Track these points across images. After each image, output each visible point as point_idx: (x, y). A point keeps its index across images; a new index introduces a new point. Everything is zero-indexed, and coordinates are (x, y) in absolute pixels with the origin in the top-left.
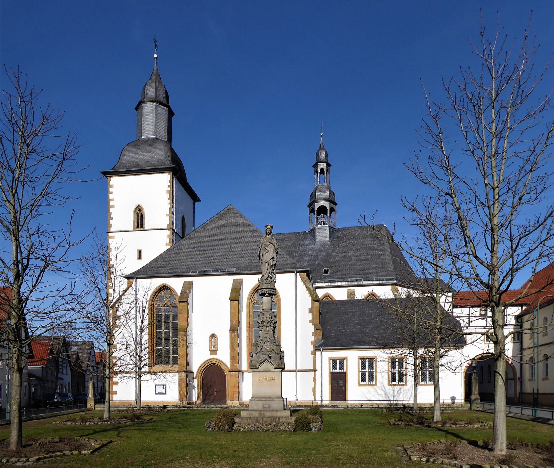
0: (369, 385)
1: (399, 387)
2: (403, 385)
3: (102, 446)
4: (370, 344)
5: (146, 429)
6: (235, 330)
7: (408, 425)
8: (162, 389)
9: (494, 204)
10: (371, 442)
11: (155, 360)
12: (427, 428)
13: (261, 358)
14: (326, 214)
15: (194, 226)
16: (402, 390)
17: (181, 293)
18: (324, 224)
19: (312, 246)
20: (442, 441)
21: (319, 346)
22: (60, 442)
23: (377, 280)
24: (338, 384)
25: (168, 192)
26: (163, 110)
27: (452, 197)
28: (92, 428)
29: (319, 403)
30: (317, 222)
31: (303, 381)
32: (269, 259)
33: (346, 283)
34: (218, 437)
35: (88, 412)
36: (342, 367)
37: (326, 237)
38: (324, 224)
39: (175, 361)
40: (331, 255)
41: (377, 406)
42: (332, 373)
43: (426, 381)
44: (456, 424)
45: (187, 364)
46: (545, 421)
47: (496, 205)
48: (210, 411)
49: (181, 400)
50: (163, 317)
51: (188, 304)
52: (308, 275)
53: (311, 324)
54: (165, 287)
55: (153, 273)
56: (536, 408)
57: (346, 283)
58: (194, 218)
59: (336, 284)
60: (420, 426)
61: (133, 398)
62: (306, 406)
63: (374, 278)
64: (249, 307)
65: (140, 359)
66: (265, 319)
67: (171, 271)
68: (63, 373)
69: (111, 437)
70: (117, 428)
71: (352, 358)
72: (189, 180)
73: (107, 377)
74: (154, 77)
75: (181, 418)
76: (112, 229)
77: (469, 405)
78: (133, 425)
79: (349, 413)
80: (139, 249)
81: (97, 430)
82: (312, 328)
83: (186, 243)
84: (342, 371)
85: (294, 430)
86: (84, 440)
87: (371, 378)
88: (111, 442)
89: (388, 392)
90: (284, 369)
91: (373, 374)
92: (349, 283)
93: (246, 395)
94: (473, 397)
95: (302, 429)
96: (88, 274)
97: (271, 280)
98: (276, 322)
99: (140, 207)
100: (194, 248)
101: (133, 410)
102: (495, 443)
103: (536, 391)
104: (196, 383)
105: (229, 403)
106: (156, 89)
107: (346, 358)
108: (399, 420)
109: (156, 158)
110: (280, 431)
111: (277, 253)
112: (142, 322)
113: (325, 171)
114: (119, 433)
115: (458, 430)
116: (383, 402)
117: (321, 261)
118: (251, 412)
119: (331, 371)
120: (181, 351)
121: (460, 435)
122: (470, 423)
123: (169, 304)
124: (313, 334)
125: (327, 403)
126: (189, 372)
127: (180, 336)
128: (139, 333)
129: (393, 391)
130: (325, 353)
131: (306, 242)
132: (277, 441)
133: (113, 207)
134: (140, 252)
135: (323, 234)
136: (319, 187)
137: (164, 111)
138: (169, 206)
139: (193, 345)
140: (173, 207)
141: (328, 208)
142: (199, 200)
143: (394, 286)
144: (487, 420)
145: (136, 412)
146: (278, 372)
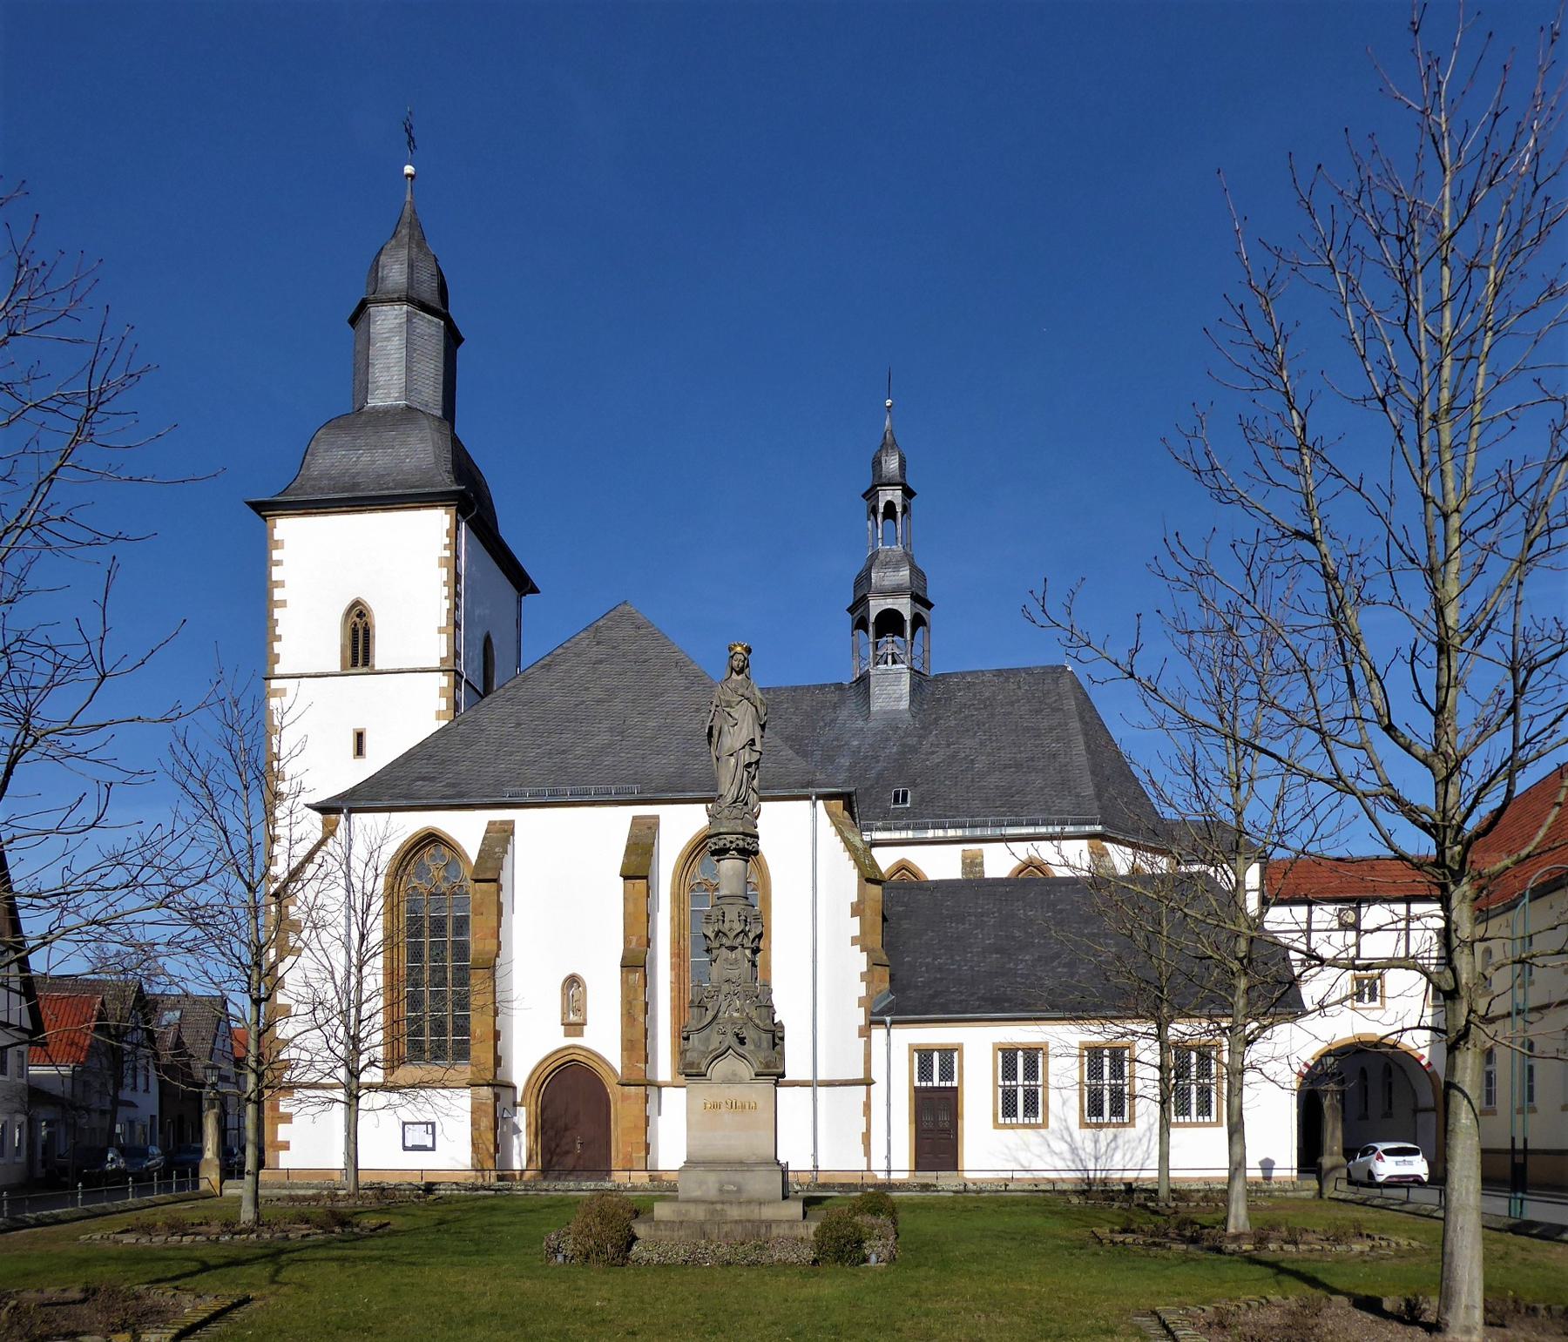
0: (1025, 1126)
1: (1112, 1130)
2: (1124, 1125)
3: (216, 1316)
4: (1025, 1006)
5: (363, 1259)
6: (636, 963)
7: (1154, 1244)
8: (422, 1136)
9: (1447, 562)
10: (1056, 1302)
11: (404, 1050)
12: (1213, 1256)
13: (714, 1044)
14: (902, 635)
15: (519, 665)
16: (1120, 1141)
17: (480, 856)
18: (894, 662)
19: (860, 723)
20: (1272, 1298)
21: (882, 1013)
22: (83, 1301)
23: (1046, 823)
24: (937, 1121)
25: (443, 562)
26: (430, 327)
27: (1314, 541)
28: (197, 1254)
29: (882, 1176)
30: (875, 655)
31: (838, 1117)
32: (738, 746)
33: (959, 833)
34: (582, 1283)
35: (200, 1203)
36: (947, 1073)
37: (899, 699)
38: (894, 662)
39: (462, 1052)
40: (914, 750)
41: (1049, 1187)
42: (917, 1090)
43: (1189, 1114)
44: (1296, 1243)
45: (497, 1061)
46: (1551, 1233)
47: (1453, 567)
48: (562, 1200)
49: (478, 1168)
50: (426, 924)
51: (500, 888)
52: (849, 807)
54: (430, 839)
55: (398, 797)
56: (1520, 1195)
57: (959, 833)
58: (519, 641)
59: (930, 834)
60: (1192, 1248)
61: (338, 1161)
62: (842, 1185)
63: (1039, 817)
64: (677, 899)
65: (355, 1047)
66: (727, 925)
67: (451, 791)
68: (135, 1088)
69: (250, 1285)
70: (274, 1256)
71: (978, 1046)
72: (507, 532)
73: (248, 1099)
74: (405, 232)
75: (474, 1223)
77: (1314, 1184)
78: (326, 1245)
79: (970, 1206)
80: (359, 726)
81: (212, 1262)
82: (860, 961)
83: (493, 711)
84: (949, 1084)
85: (815, 1262)
86: (161, 1296)
87: (1031, 1107)
88: (247, 1300)
89: (1079, 1144)
90: (783, 1075)
91: (1036, 1093)
92: (968, 833)
93: (671, 1146)
94: (1327, 1161)
95: (840, 1257)
96: (193, 786)
97: (746, 809)
98: (760, 936)
99: (362, 604)
101: (333, 1197)
102: (1447, 1308)
103: (1519, 1145)
104: (521, 1118)
105: (619, 1177)
106: (411, 266)
107: (958, 1048)
108: (1124, 1231)
110: (772, 1265)
111: (763, 727)
112: (363, 937)
113: (899, 509)
114: (277, 1272)
115: (1306, 1260)
116: (1064, 1175)
117: (886, 769)
118: (684, 1207)
119: (917, 1084)
120: (478, 1025)
121: (1320, 1276)
122: (1338, 1240)
123: (444, 886)
124: (863, 976)
125: (905, 1176)
126: (501, 1087)
127: (477, 980)
128: (353, 970)
129: (1096, 1142)
130: (897, 1032)
131: (843, 714)
132: (766, 1298)
133: (283, 604)
134: (360, 736)
135: (892, 691)
136: (882, 557)
137: (433, 330)
138: (447, 604)
139: (515, 1005)
140: (457, 607)
141: (907, 616)
142: (535, 590)
143: (1097, 842)
144: (1382, 1230)
145: (341, 1204)
146: (765, 1086)
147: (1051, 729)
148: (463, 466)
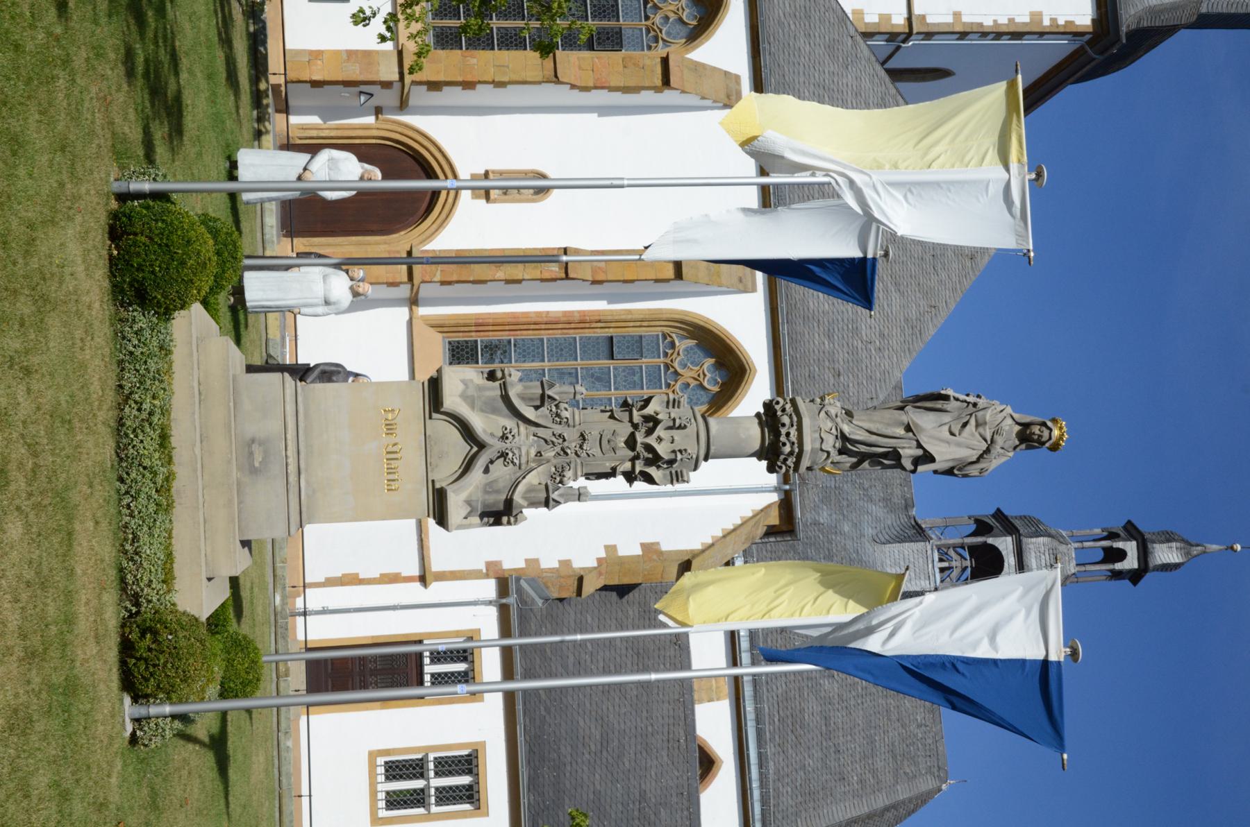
0: (373, 793)
6: (555, 267)
18: (942, 570)
19: (869, 532)
21: (520, 591)
24: (383, 671)
25: (1037, 16)
38: (942, 570)
39: (446, 39)
53: (603, 555)
71: (474, 722)
98: (649, 479)
111: (949, 472)
113: (1118, 566)
119: (431, 757)
124: (566, 563)
127: (527, 60)
131: (878, 510)
136: (1063, 548)
138: (988, 22)
140: (984, 35)
147: (874, 772)
148: (1148, 37)
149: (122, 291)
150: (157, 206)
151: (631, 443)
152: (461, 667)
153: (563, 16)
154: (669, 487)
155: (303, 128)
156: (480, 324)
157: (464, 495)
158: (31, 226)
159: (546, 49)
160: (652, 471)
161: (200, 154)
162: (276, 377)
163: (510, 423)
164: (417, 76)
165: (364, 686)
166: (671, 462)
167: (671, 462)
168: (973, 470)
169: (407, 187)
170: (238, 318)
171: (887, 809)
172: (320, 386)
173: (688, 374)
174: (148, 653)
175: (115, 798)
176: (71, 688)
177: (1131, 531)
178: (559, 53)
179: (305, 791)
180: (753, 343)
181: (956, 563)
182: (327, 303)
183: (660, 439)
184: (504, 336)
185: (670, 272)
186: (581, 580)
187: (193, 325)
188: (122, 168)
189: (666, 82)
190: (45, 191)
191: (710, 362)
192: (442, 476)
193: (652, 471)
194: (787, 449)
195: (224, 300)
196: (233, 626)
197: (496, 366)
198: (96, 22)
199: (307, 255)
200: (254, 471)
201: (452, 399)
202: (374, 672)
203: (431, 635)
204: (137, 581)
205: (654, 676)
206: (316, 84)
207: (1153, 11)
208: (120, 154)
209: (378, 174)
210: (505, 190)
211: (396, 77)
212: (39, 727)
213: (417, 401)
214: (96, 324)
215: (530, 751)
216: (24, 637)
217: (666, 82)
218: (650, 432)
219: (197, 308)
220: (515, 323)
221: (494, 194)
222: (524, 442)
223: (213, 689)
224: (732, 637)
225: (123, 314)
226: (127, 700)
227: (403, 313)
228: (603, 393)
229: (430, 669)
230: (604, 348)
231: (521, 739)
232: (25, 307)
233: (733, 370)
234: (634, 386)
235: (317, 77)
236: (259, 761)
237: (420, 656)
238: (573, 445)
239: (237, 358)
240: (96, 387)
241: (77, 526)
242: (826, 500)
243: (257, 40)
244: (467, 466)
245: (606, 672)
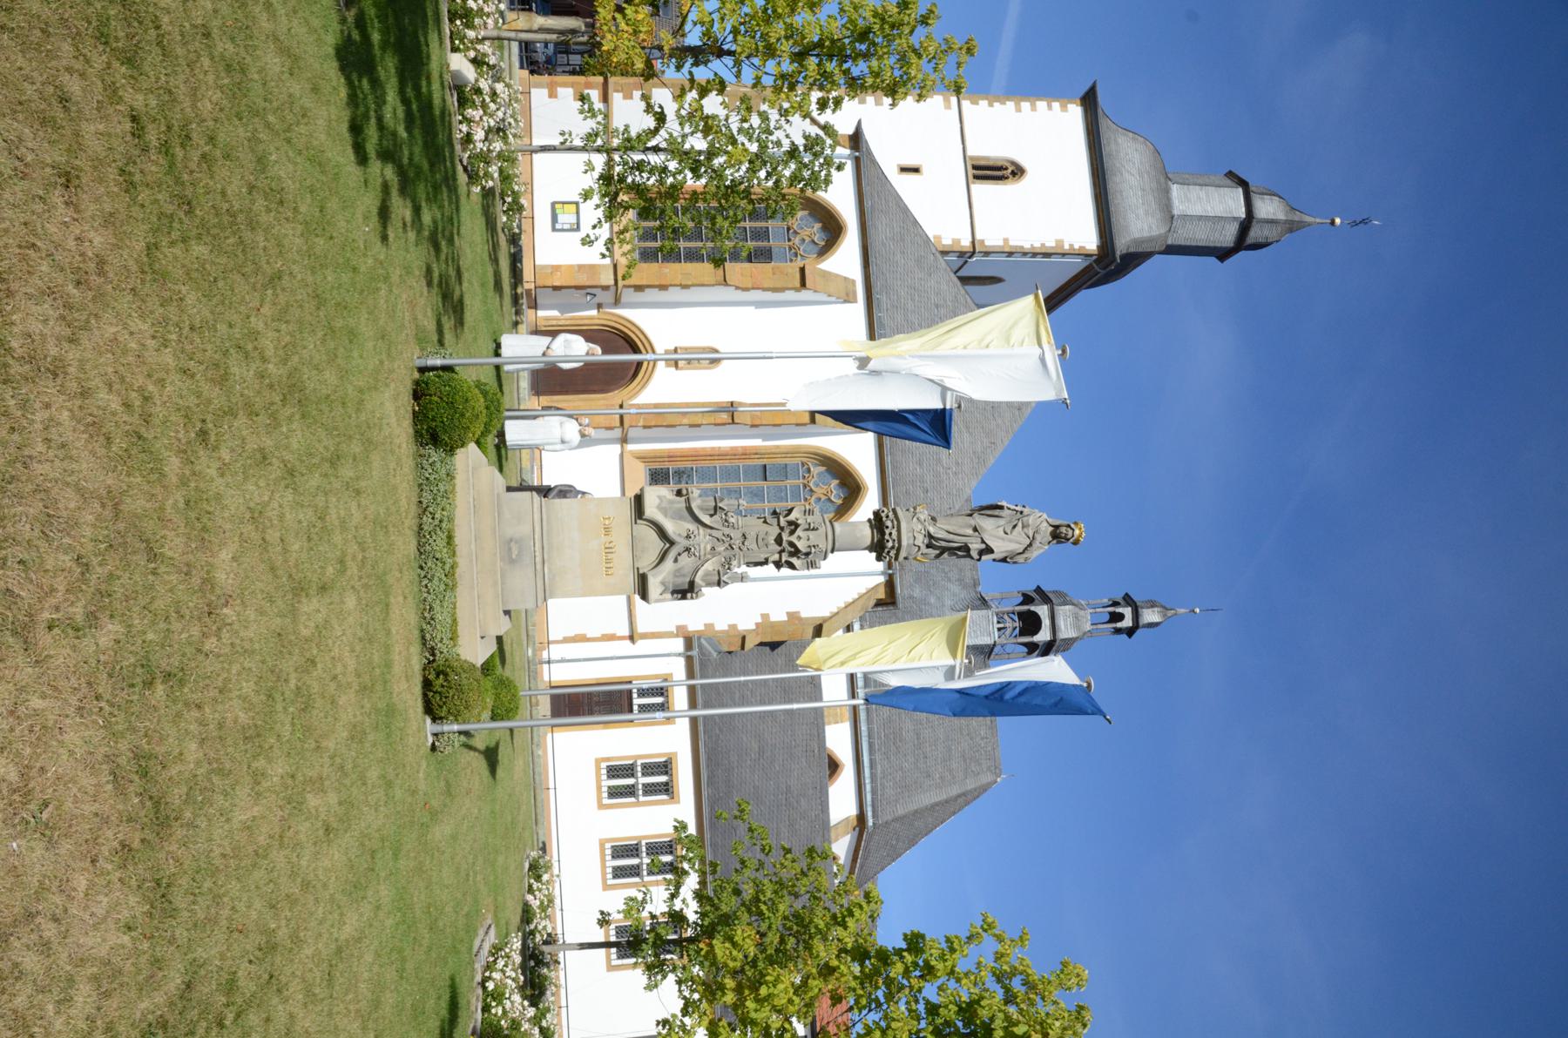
0: (599, 788)
6: (729, 415)
14: (1022, 634)
19: (948, 603)
21: (700, 646)
25: (1060, 243)
26: (1228, 237)
39: (648, 256)
71: (669, 739)
76: (966, 104)
80: (924, 170)
98: (792, 566)
100: (937, 306)
109: (1131, 217)
111: (1004, 560)
113: (1119, 625)
120: (673, 271)
124: (733, 627)
127: (705, 269)
131: (955, 588)
133: (1018, 110)
134: (916, 170)
138: (1027, 246)
140: (1025, 254)
147: (950, 771)
148: (1134, 259)
149: (421, 436)
150: (446, 375)
151: (779, 540)
152: (659, 700)
153: (729, 238)
154: (806, 572)
155: (547, 319)
156: (671, 456)
157: (660, 578)
158: (361, 391)
159: (718, 262)
160: (794, 560)
161: (475, 339)
162: (527, 494)
163: (692, 526)
164: (627, 282)
165: (591, 713)
166: (807, 554)
167: (807, 554)
168: (1020, 559)
169: (618, 361)
170: (500, 452)
171: (959, 796)
172: (558, 501)
173: (820, 491)
174: (440, 690)
175: (422, 786)
176: (391, 711)
177: (1128, 600)
178: (727, 264)
179: (551, 785)
180: (867, 471)
181: (1009, 624)
182: (563, 442)
183: (799, 538)
184: (688, 465)
185: (807, 419)
186: (744, 638)
187: (470, 460)
188: (422, 349)
189: (803, 284)
190: (371, 367)
191: (836, 482)
192: (645, 564)
193: (794, 560)
194: (890, 544)
195: (491, 440)
196: (499, 670)
197: (682, 486)
198: (407, 251)
199: (549, 408)
200: (512, 561)
201: (651, 510)
202: (598, 704)
203: (637, 678)
204: (433, 638)
205: (795, 706)
206: (556, 288)
207: (1138, 242)
208: (421, 340)
209: (598, 350)
210: (689, 361)
211: (612, 282)
212: (371, 737)
213: (627, 511)
214: (404, 459)
215: (709, 759)
216: (358, 676)
217: (803, 284)
218: (792, 533)
219: (472, 446)
220: (696, 455)
221: (681, 363)
222: (703, 540)
223: (486, 714)
224: (852, 678)
225: (422, 451)
226: (429, 720)
227: (617, 448)
228: (759, 505)
229: (637, 701)
230: (760, 473)
231: (702, 750)
232: (356, 448)
233: (851, 488)
234: (781, 500)
235: (557, 283)
236: (519, 763)
237: (630, 692)
238: (737, 542)
239: (500, 481)
240: (404, 502)
241: (392, 600)
242: (918, 580)
243: (516, 259)
244: (662, 557)
245: (762, 703)
